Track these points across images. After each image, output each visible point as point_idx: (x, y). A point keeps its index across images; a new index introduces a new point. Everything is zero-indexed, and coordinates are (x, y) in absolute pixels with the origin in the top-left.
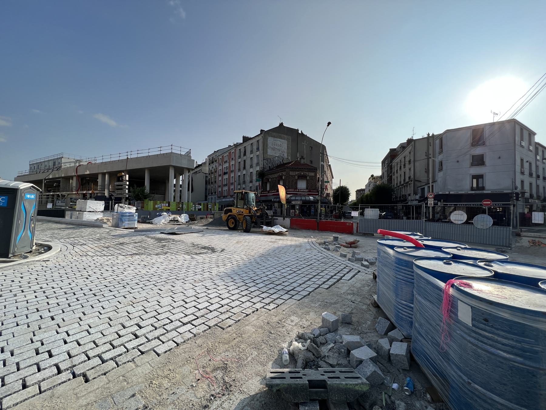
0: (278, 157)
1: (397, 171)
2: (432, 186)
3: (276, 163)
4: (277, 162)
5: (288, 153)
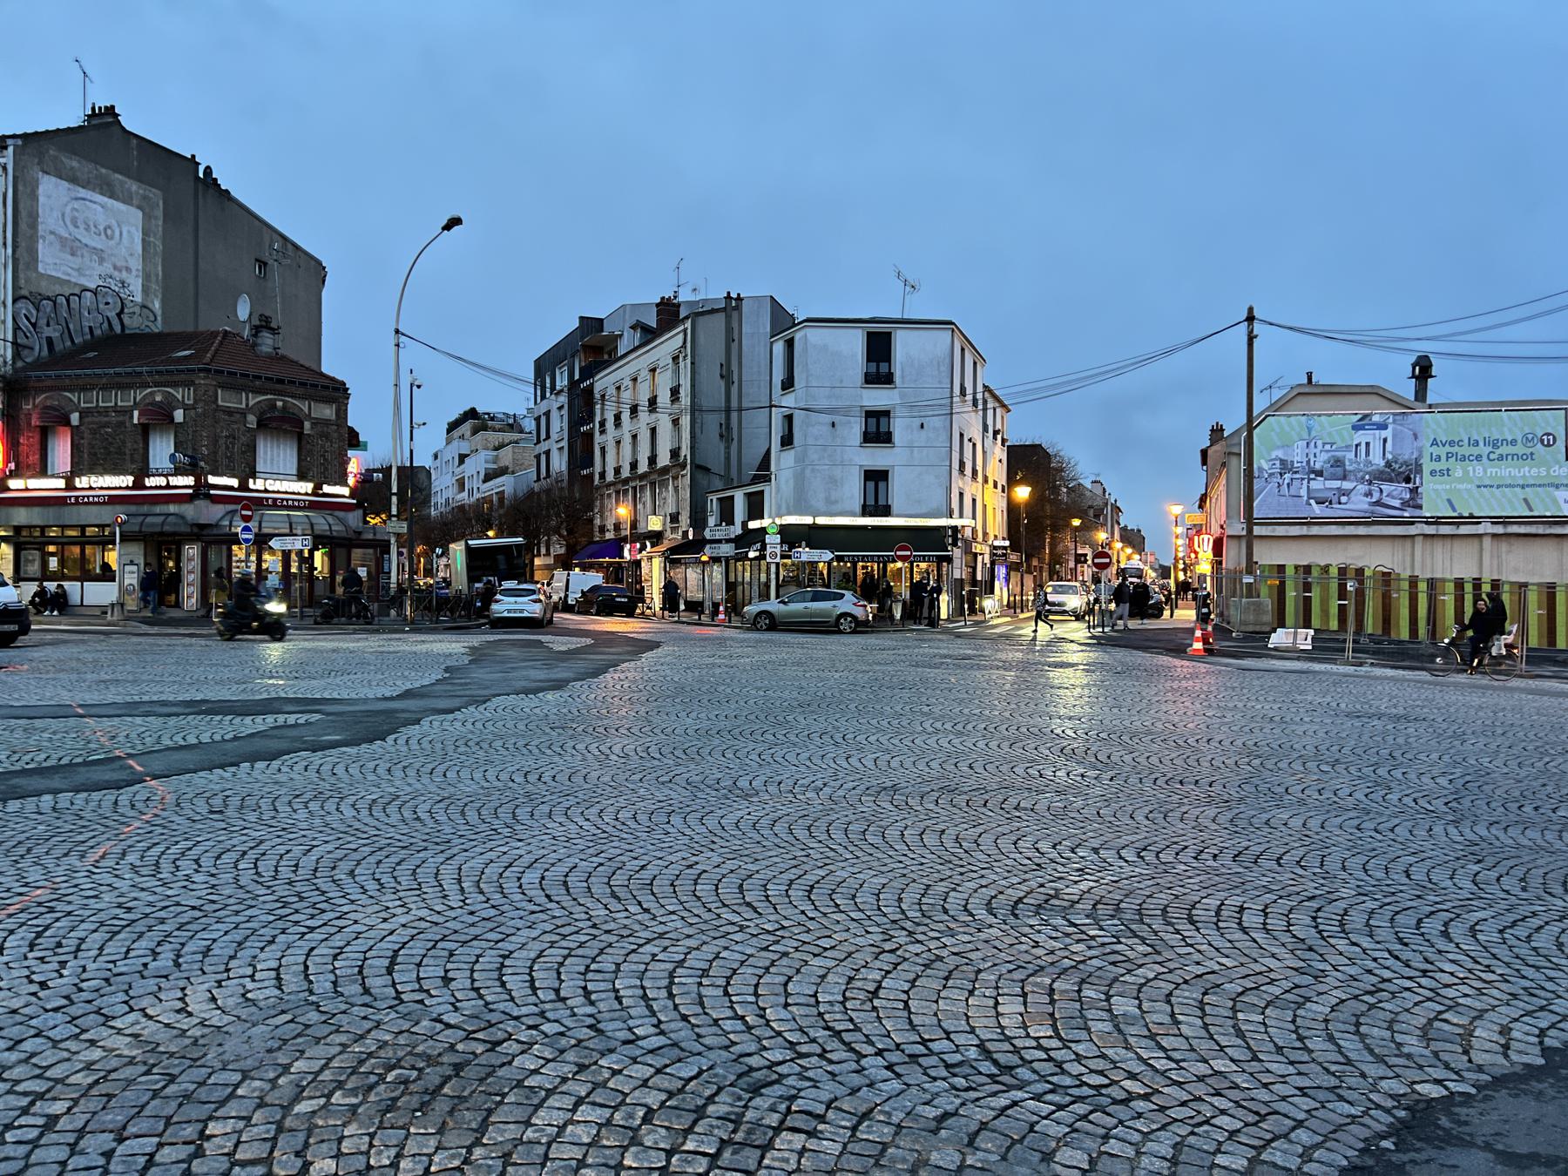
0: (95, 293)
1: (618, 417)
4: (90, 320)
5: (147, 277)
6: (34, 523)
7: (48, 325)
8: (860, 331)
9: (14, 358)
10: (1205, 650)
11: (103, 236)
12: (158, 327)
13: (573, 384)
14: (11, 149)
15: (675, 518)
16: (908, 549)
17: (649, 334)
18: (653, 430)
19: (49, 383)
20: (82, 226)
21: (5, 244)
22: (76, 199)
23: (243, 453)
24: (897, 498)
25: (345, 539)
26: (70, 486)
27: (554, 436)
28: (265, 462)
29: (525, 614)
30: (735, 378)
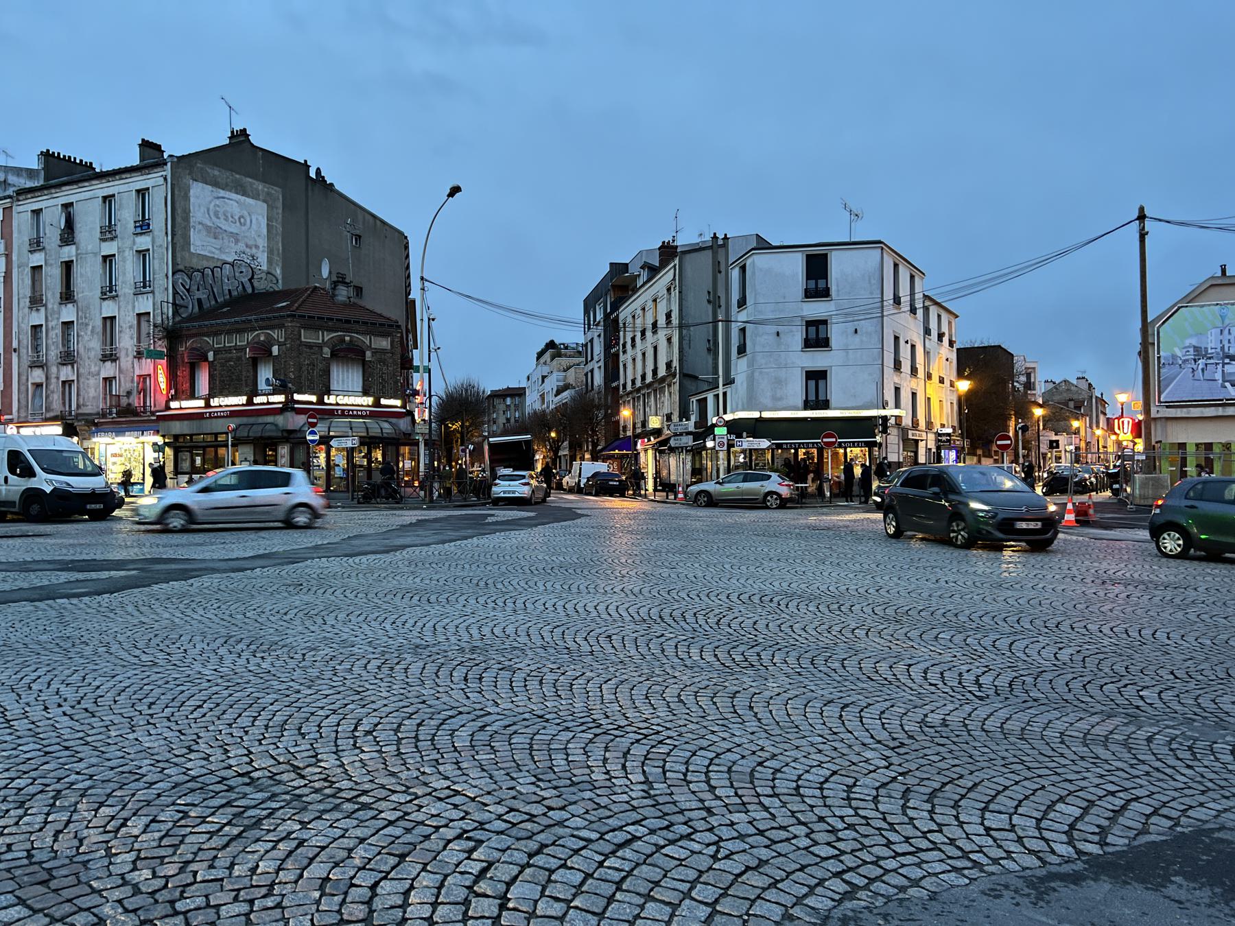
0: (232, 265)
1: (633, 339)
2: (725, 394)
3: (226, 288)
4: (229, 285)
5: (271, 252)
6: (185, 433)
7: (198, 290)
8: (799, 255)
9: (173, 315)
10: (1077, 521)
11: (238, 223)
12: (280, 287)
13: (607, 316)
14: (169, 164)
15: (669, 417)
16: (834, 437)
17: (653, 271)
18: (655, 348)
19: (194, 331)
20: (222, 217)
21: (167, 233)
22: (218, 198)
23: (321, 376)
24: (834, 395)
25: (394, 439)
26: (208, 405)
27: (596, 358)
28: (338, 383)
29: (517, 495)
30: (723, 302)
